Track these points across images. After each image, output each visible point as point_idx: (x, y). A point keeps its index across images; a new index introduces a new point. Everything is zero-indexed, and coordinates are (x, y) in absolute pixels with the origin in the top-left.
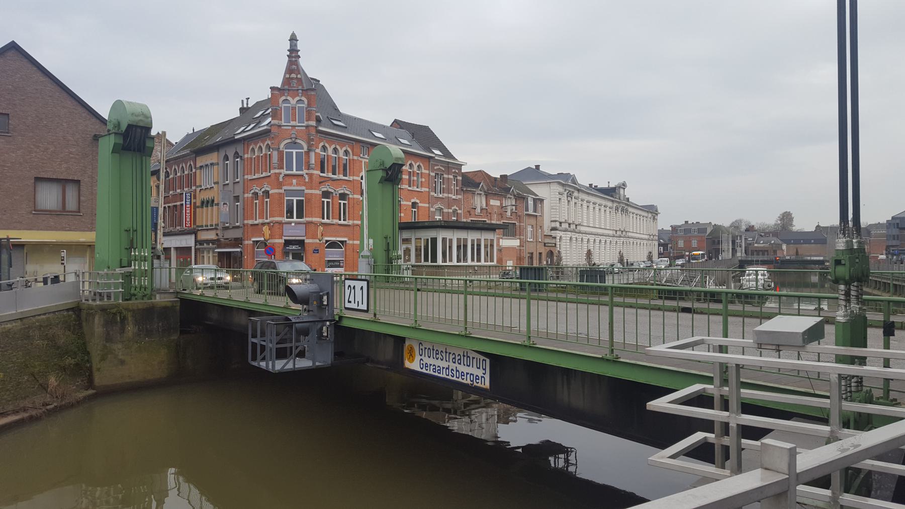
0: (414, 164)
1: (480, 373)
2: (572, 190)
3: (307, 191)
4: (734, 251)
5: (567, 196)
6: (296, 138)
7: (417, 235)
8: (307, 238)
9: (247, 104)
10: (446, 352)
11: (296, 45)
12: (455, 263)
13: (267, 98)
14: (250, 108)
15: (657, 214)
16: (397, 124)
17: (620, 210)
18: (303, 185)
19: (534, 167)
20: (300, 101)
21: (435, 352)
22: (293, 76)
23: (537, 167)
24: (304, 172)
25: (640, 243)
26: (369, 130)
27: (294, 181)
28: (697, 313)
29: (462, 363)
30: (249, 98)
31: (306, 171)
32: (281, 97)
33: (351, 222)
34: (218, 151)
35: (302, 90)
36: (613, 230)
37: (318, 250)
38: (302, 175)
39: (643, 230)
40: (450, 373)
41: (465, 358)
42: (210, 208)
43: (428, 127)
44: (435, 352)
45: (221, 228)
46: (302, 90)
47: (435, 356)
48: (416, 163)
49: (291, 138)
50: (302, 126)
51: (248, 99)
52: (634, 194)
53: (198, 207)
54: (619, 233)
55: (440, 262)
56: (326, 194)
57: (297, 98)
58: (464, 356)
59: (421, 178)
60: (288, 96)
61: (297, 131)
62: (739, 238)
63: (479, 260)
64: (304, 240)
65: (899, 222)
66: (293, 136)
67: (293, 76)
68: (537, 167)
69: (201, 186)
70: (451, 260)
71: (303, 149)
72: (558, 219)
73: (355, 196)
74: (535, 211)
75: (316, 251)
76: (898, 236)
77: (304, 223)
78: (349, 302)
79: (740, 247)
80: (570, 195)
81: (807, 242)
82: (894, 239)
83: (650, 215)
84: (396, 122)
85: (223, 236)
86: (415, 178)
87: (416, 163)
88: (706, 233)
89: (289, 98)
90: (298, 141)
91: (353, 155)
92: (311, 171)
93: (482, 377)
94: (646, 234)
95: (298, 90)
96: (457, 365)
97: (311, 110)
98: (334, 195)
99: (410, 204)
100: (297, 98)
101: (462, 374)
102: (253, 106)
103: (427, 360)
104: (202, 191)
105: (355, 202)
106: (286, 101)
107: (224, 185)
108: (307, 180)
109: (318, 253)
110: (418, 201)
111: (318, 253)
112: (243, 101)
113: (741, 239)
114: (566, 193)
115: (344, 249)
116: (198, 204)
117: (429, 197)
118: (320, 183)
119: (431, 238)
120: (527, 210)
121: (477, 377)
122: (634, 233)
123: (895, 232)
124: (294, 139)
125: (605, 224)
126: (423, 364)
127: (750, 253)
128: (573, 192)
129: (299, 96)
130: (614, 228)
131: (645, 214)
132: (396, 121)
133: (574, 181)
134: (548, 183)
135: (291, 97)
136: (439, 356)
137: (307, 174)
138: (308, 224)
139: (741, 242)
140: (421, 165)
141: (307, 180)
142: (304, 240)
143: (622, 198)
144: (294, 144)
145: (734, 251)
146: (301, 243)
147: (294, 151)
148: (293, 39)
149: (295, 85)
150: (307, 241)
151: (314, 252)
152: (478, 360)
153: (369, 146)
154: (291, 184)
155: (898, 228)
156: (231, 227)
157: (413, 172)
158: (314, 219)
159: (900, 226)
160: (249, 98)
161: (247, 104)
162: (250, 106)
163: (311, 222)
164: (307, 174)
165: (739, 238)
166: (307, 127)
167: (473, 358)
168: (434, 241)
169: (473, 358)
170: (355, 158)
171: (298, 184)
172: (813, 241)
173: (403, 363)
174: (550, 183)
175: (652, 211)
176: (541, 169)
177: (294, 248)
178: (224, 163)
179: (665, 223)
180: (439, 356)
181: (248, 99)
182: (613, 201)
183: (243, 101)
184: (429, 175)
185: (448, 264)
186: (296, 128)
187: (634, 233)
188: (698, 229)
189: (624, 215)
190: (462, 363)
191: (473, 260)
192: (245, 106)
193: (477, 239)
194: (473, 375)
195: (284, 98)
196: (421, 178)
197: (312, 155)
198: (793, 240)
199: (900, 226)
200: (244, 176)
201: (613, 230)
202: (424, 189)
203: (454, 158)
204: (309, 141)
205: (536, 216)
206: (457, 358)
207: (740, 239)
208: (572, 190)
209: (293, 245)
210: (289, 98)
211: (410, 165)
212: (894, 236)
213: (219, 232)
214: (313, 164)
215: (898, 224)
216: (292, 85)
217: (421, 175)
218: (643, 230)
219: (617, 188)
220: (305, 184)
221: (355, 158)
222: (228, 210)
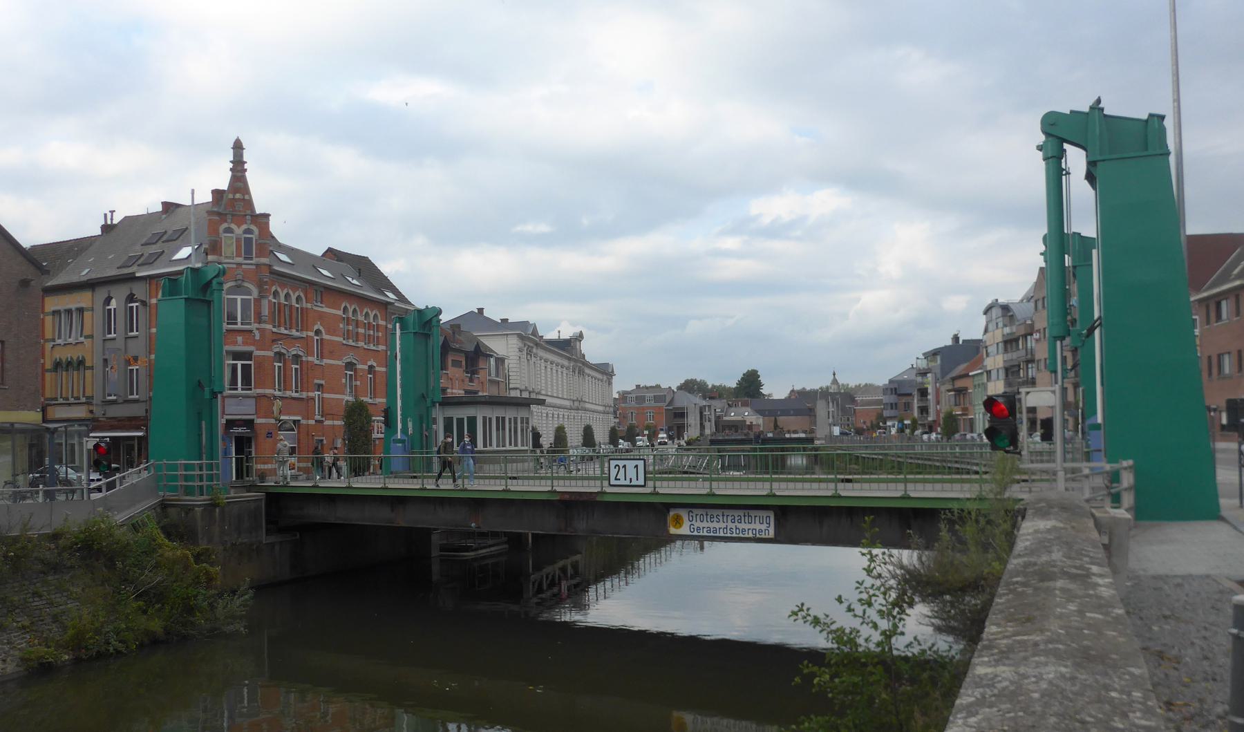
0: (370, 312)
1: (763, 527)
2: (531, 345)
3: (257, 353)
4: (702, 427)
5: (527, 354)
6: (243, 281)
7: (446, 413)
8: (258, 418)
9: (112, 219)
10: (723, 515)
11: (242, 156)
12: (494, 447)
13: (146, 213)
14: (116, 225)
15: (612, 376)
16: (331, 253)
17: (577, 372)
18: (251, 344)
19: (476, 311)
20: (248, 231)
21: (709, 516)
22: (238, 196)
23: (481, 310)
24: (254, 326)
25: (553, 414)
26: (342, 274)
27: (240, 339)
28: (856, 482)
29: (743, 521)
30: (114, 211)
31: (257, 325)
32: (221, 224)
33: (304, 395)
34: (93, 291)
35: (251, 216)
36: (570, 400)
37: (271, 433)
38: (251, 331)
39: (563, 391)
40: (729, 531)
41: (747, 518)
42: (64, 373)
43: (367, 257)
44: (709, 516)
45: (100, 403)
46: (251, 216)
47: (709, 520)
48: (372, 311)
49: (236, 281)
50: (251, 264)
51: (112, 212)
52: (592, 350)
53: (48, 371)
54: (576, 404)
55: (480, 446)
56: (279, 356)
57: (244, 227)
58: (744, 516)
59: (377, 331)
60: (231, 222)
61: (244, 271)
62: (707, 408)
63: (516, 445)
64: (253, 420)
65: (897, 387)
66: (239, 277)
67: (238, 196)
68: (481, 310)
69: (53, 340)
70: (491, 445)
71: (251, 295)
72: (518, 386)
73: (310, 359)
74: (497, 375)
75: (269, 435)
76: (896, 404)
77: (254, 397)
78: (616, 479)
79: (709, 421)
80: (529, 353)
81: (786, 413)
82: (892, 408)
83: (605, 378)
84: (330, 251)
85: (103, 414)
86: (371, 332)
87: (372, 311)
88: (665, 402)
89: (233, 226)
90: (246, 284)
91: (307, 303)
92: (263, 326)
93: (765, 530)
94: (601, 405)
95: (246, 215)
96: (736, 523)
97: (265, 244)
98: (287, 357)
99: (366, 367)
100: (244, 227)
101: (744, 530)
102: (119, 223)
103: (697, 524)
104: (57, 348)
105: (309, 367)
106: (228, 230)
107: (104, 340)
108: (257, 337)
109: (271, 437)
110: (375, 364)
111: (271, 437)
112: (105, 215)
113: (709, 410)
114: (525, 348)
115: (296, 432)
116: (48, 366)
117: (386, 358)
118: (274, 341)
119: (468, 417)
120: (490, 375)
121: (760, 531)
122: (559, 398)
123: (892, 399)
124: (240, 282)
125: (563, 394)
126: (694, 528)
127: (721, 428)
128: (532, 347)
129: (246, 223)
130: (572, 397)
131: (599, 376)
132: (330, 250)
133: (535, 332)
134: (504, 334)
135: (236, 224)
136: (715, 519)
137: (257, 329)
138: (258, 397)
139: (711, 414)
140: (357, 308)
141: (257, 337)
142: (253, 420)
143: (578, 355)
144: (238, 289)
145: (702, 427)
146: (249, 423)
147: (239, 298)
148: (238, 147)
149: (241, 209)
150: (258, 421)
151: (267, 437)
152: (761, 518)
153: (322, 289)
154: (235, 343)
155: (896, 393)
156: (121, 401)
157: (369, 323)
158: (268, 391)
159: (898, 392)
160: (114, 211)
161: (112, 219)
162: (115, 222)
163: (264, 396)
164: (257, 329)
165: (707, 408)
166: (257, 265)
167: (755, 517)
168: (472, 421)
169: (755, 517)
170: (309, 306)
171: (245, 343)
172: (792, 412)
173: (668, 531)
174: (507, 335)
175: (605, 371)
176: (486, 314)
177: (240, 431)
178: (104, 309)
179: (621, 384)
180: (715, 519)
181: (112, 212)
182: (569, 359)
183: (105, 215)
184: (386, 327)
185: (489, 448)
186: (243, 266)
187: (559, 398)
188: (655, 396)
189: (581, 378)
190: (743, 521)
191: (510, 444)
192: (109, 222)
193: (468, 417)
194: (756, 530)
195: (225, 225)
196: (377, 331)
197: (265, 303)
198: (793, 410)
199: (898, 392)
200: (150, 328)
201: (570, 400)
202: (381, 348)
203: (409, 303)
204: (260, 285)
205: (498, 382)
206: (736, 519)
207: (709, 411)
208: (531, 345)
209: (239, 426)
210: (233, 226)
211: (344, 309)
212: (892, 404)
213: (94, 408)
214: (266, 316)
215: (896, 389)
216: (237, 209)
217: (377, 328)
218: (563, 391)
219: (572, 340)
220: (254, 343)
221: (309, 306)
222: (116, 376)
